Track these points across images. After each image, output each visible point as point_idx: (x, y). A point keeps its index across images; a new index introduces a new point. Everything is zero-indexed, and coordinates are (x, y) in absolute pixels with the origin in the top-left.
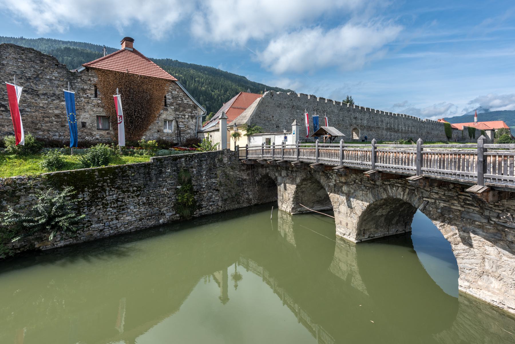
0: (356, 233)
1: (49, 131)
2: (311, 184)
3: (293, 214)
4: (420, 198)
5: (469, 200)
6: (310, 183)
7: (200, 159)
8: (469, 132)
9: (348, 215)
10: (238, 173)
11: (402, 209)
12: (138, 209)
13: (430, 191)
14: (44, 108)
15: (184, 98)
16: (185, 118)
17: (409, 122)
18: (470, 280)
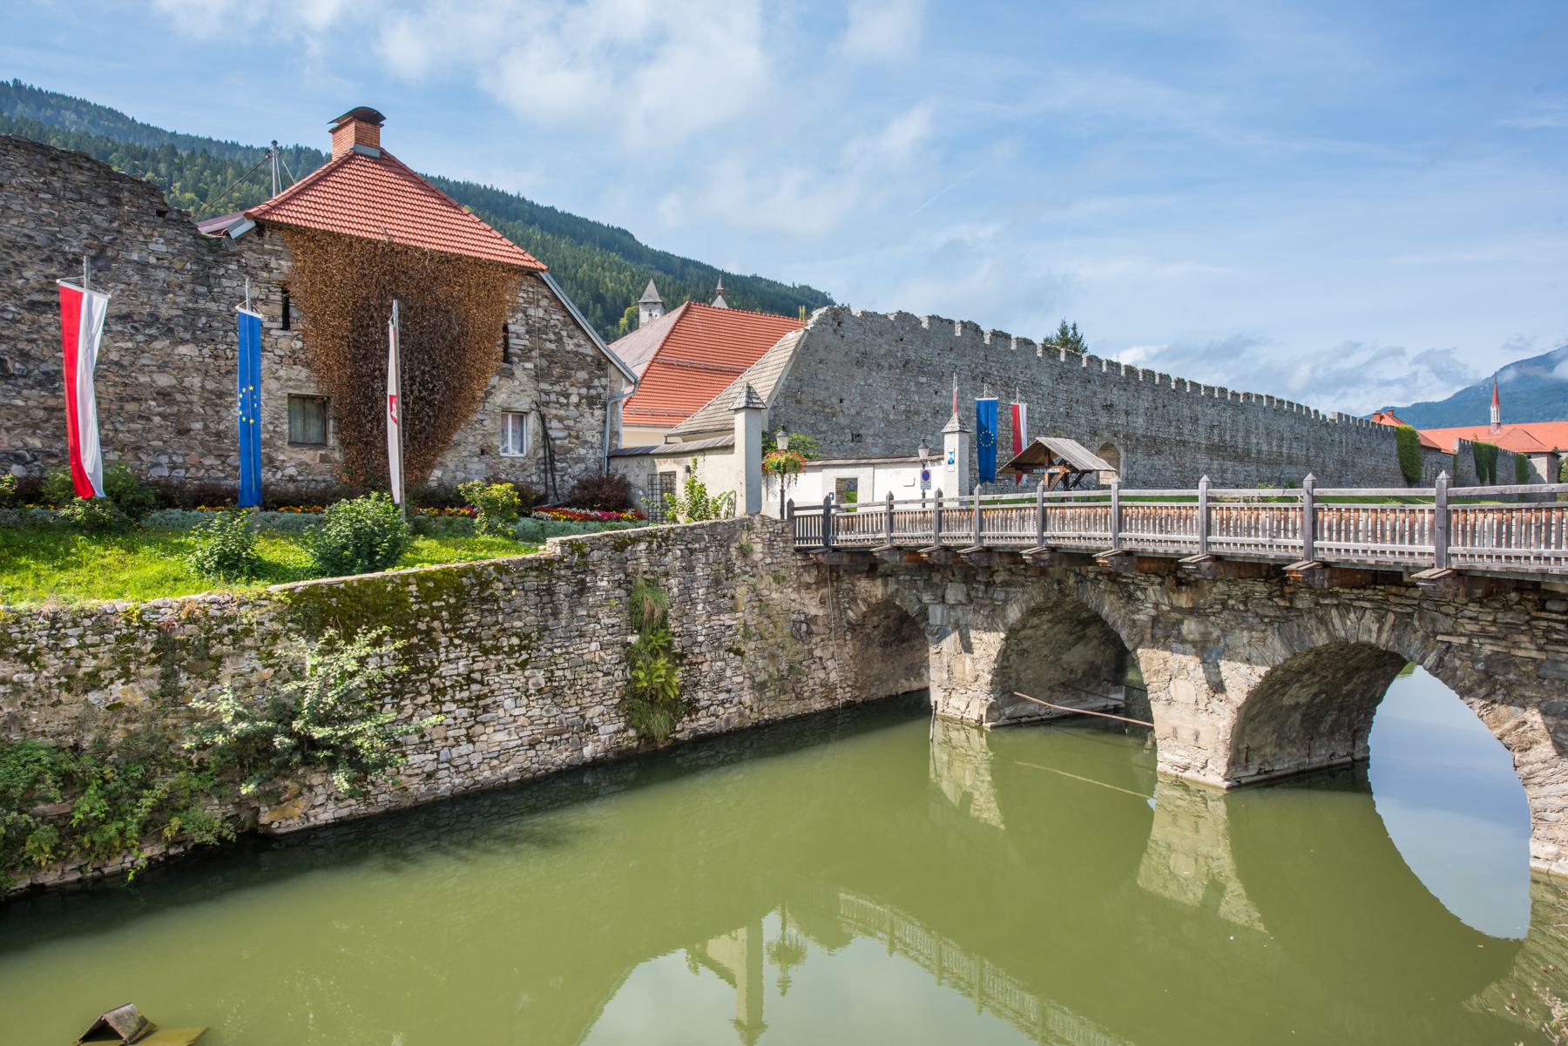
0: (1226, 760)
1: (139, 448)
2: (1049, 625)
3: (992, 727)
4: (1426, 637)
5: (1558, 631)
6: (1048, 621)
7: (689, 546)
8: (1476, 461)
9: (1202, 706)
10: (793, 596)
11: (1349, 687)
12: (523, 710)
13: (1457, 614)
14: (122, 366)
15: (564, 333)
16: (568, 405)
17: (1283, 424)
18: (1561, 839)
